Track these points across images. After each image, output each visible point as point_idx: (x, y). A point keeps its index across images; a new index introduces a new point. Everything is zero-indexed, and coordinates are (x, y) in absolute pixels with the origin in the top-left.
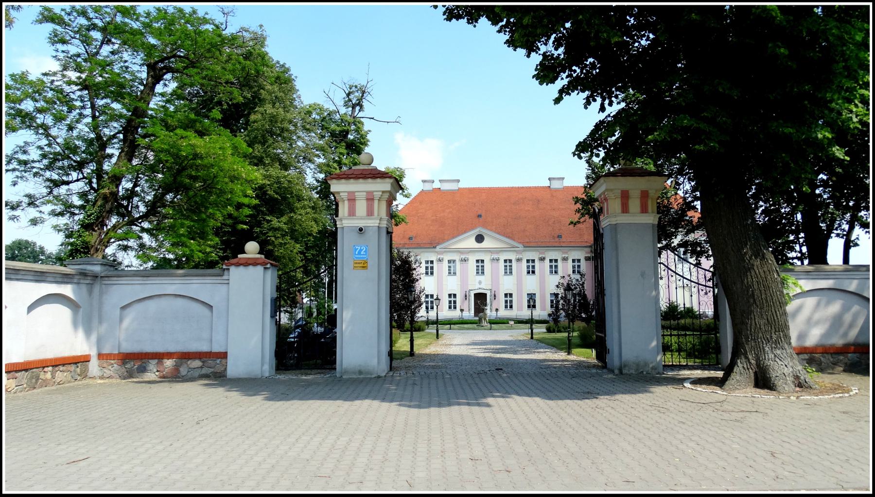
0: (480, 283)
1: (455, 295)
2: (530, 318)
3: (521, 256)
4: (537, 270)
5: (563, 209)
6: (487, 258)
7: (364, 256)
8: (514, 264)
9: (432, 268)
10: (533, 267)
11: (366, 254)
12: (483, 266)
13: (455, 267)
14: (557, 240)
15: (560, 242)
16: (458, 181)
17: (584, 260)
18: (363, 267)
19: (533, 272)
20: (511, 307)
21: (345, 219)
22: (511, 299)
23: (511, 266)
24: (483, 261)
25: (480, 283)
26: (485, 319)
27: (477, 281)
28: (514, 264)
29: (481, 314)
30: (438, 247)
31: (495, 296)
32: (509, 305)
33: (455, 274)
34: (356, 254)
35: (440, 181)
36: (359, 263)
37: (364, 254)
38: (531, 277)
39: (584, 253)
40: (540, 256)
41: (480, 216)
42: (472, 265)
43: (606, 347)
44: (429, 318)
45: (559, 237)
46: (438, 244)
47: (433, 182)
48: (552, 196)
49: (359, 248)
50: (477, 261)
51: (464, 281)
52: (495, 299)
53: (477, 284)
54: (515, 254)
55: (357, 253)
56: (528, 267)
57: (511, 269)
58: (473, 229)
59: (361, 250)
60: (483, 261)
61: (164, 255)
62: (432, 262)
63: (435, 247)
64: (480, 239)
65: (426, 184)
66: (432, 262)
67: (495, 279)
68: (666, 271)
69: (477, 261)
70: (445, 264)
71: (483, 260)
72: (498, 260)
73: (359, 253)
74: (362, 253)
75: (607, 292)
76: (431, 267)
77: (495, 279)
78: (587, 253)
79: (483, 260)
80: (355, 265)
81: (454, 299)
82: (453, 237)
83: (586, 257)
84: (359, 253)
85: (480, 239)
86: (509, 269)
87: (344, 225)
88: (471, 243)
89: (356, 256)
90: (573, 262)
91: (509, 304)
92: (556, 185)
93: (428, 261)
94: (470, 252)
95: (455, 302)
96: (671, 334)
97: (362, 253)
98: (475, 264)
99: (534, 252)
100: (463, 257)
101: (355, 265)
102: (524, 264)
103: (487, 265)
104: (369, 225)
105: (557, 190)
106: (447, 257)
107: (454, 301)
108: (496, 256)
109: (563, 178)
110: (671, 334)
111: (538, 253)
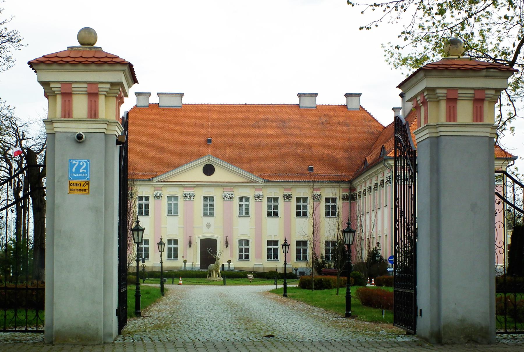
0: (208, 226)
1: (176, 242)
3: (261, 194)
4: (280, 211)
5: (315, 134)
6: (217, 194)
7: (84, 175)
8: (252, 203)
9: (147, 206)
10: (276, 207)
11: (87, 173)
12: (212, 205)
14: (307, 173)
15: (310, 176)
16: (181, 95)
17: (341, 199)
18: (83, 190)
19: (276, 214)
20: (247, 257)
21: (58, 121)
23: (247, 206)
24: (212, 198)
25: (208, 226)
26: (216, 271)
28: (252, 202)
30: (155, 180)
31: (227, 243)
32: (244, 255)
33: (176, 214)
34: (72, 172)
35: (159, 94)
36: (78, 185)
37: (83, 173)
38: (273, 220)
39: (341, 190)
40: (285, 193)
41: (209, 141)
42: (198, 204)
43: (416, 308)
44: (146, 270)
45: (311, 169)
46: (156, 176)
47: (149, 95)
48: (302, 117)
49: (77, 163)
50: (205, 198)
51: (188, 223)
54: (253, 190)
55: (74, 170)
56: (269, 207)
57: (247, 210)
58: (199, 157)
59: (79, 166)
60: (212, 198)
62: (147, 198)
63: (151, 180)
64: (209, 170)
65: (141, 97)
66: (147, 198)
67: (228, 224)
68: (501, 204)
69: (205, 198)
70: (164, 201)
73: (77, 170)
74: (81, 171)
75: (117, 290)
77: (228, 224)
78: (344, 190)
80: (71, 187)
81: (175, 246)
82: (175, 168)
83: (343, 196)
84: (77, 170)
85: (209, 170)
86: (207, 210)
87: (56, 130)
88: (198, 175)
89: (74, 174)
92: (307, 103)
94: (197, 186)
96: (26, 329)
97: (81, 171)
98: (202, 202)
99: (278, 189)
101: (71, 187)
102: (265, 203)
103: (218, 204)
104: (91, 131)
105: (308, 110)
106: (167, 192)
107: (332, 206)
108: (229, 193)
109: (316, 95)
110: (26, 329)
111: (282, 190)
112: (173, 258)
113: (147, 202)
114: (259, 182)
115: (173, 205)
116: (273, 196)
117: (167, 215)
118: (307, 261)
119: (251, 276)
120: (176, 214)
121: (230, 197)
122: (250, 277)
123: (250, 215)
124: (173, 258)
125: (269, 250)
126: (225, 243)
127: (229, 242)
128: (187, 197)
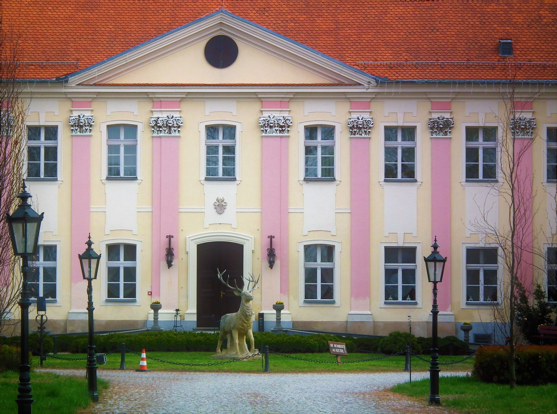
0: (220, 206)
2: (87, 330)
3: (367, 116)
12: (230, 150)
13: (132, 150)
20: (328, 293)
22: (129, 264)
25: (220, 206)
27: (211, 200)
29: (231, 316)
30: (74, 80)
33: (131, 175)
46: (76, 70)
52: (170, 264)
53: (210, 210)
54: (345, 107)
57: (329, 162)
58: (195, 18)
61: (526, 124)
63: (62, 80)
71: (233, 128)
72: (284, 127)
76: (47, 149)
79: (233, 128)
86: (216, 163)
90: (387, 138)
91: (122, 283)
93: (395, 128)
94: (189, 97)
95: (131, 274)
100: (163, 115)
107: (126, 269)
111: (427, 105)
112: (122, 297)
113: (50, 143)
114: (360, 84)
115: (122, 149)
116: (400, 122)
117: (206, 179)
118: (498, 304)
119: (339, 346)
120: (131, 175)
121: (281, 127)
122: (337, 351)
123: (337, 175)
124: (122, 297)
125: (390, 274)
126: (267, 253)
127: (277, 252)
128: (160, 127)
